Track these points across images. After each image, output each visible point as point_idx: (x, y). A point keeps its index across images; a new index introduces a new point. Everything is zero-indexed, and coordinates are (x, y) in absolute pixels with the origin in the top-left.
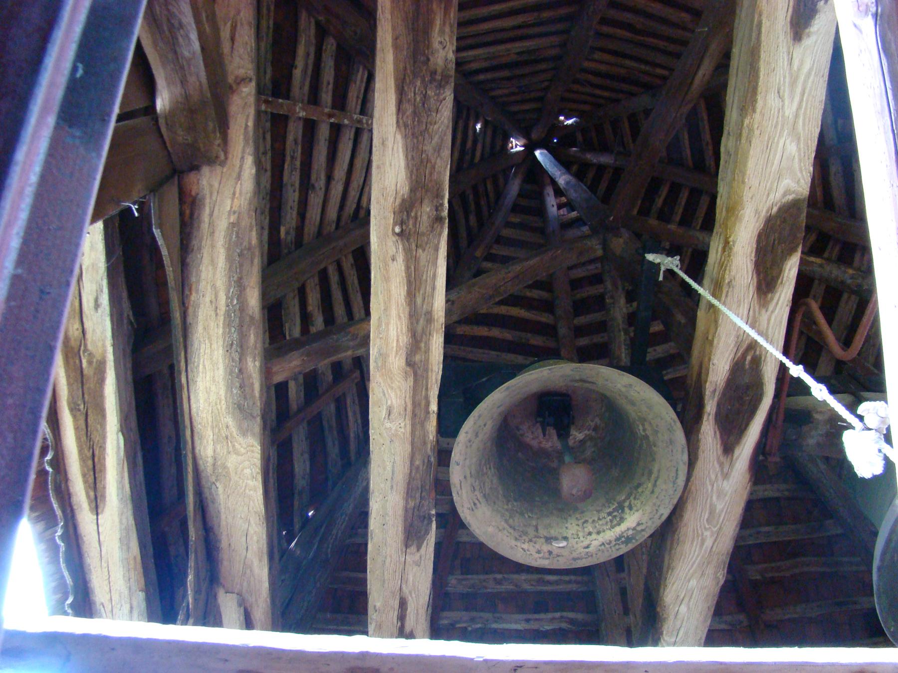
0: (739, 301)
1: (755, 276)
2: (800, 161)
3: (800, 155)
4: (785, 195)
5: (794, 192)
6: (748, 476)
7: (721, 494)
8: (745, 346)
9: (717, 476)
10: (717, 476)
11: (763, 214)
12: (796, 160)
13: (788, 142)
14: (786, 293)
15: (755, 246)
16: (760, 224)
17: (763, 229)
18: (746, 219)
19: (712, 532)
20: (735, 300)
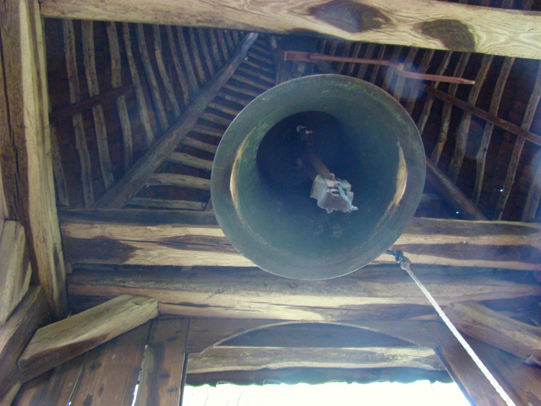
0: (419, 10)
1: (434, 20)
2: (494, 45)
3: (498, 44)
4: (478, 36)
5: (479, 42)
6: (290, 28)
7: (277, 9)
8: (389, 16)
9: (292, 4)
10: (292, 4)
11: (470, 23)
12: (496, 43)
13: (506, 36)
14: (420, 42)
15: (452, 19)
16: (464, 22)
17: (461, 24)
18: (468, 12)
19: (243, 5)
20: (420, 8)
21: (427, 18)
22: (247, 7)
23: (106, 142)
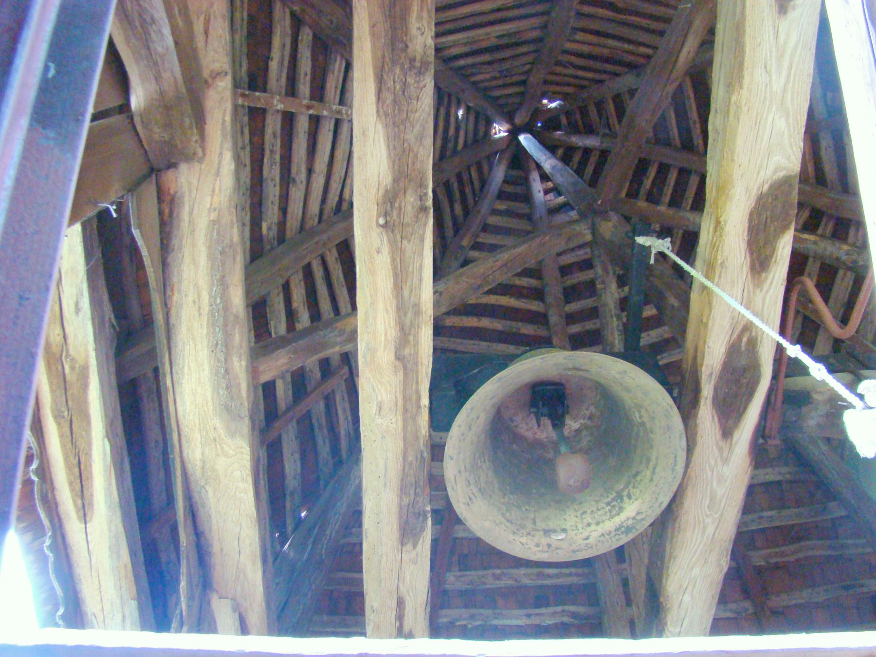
1: (748, 255)
4: (775, 171)
5: (784, 169)
6: (748, 460)
12: (786, 135)
13: (777, 117)
15: (747, 225)
21: (744, 269)
22: (716, 513)
23: (784, 513)
